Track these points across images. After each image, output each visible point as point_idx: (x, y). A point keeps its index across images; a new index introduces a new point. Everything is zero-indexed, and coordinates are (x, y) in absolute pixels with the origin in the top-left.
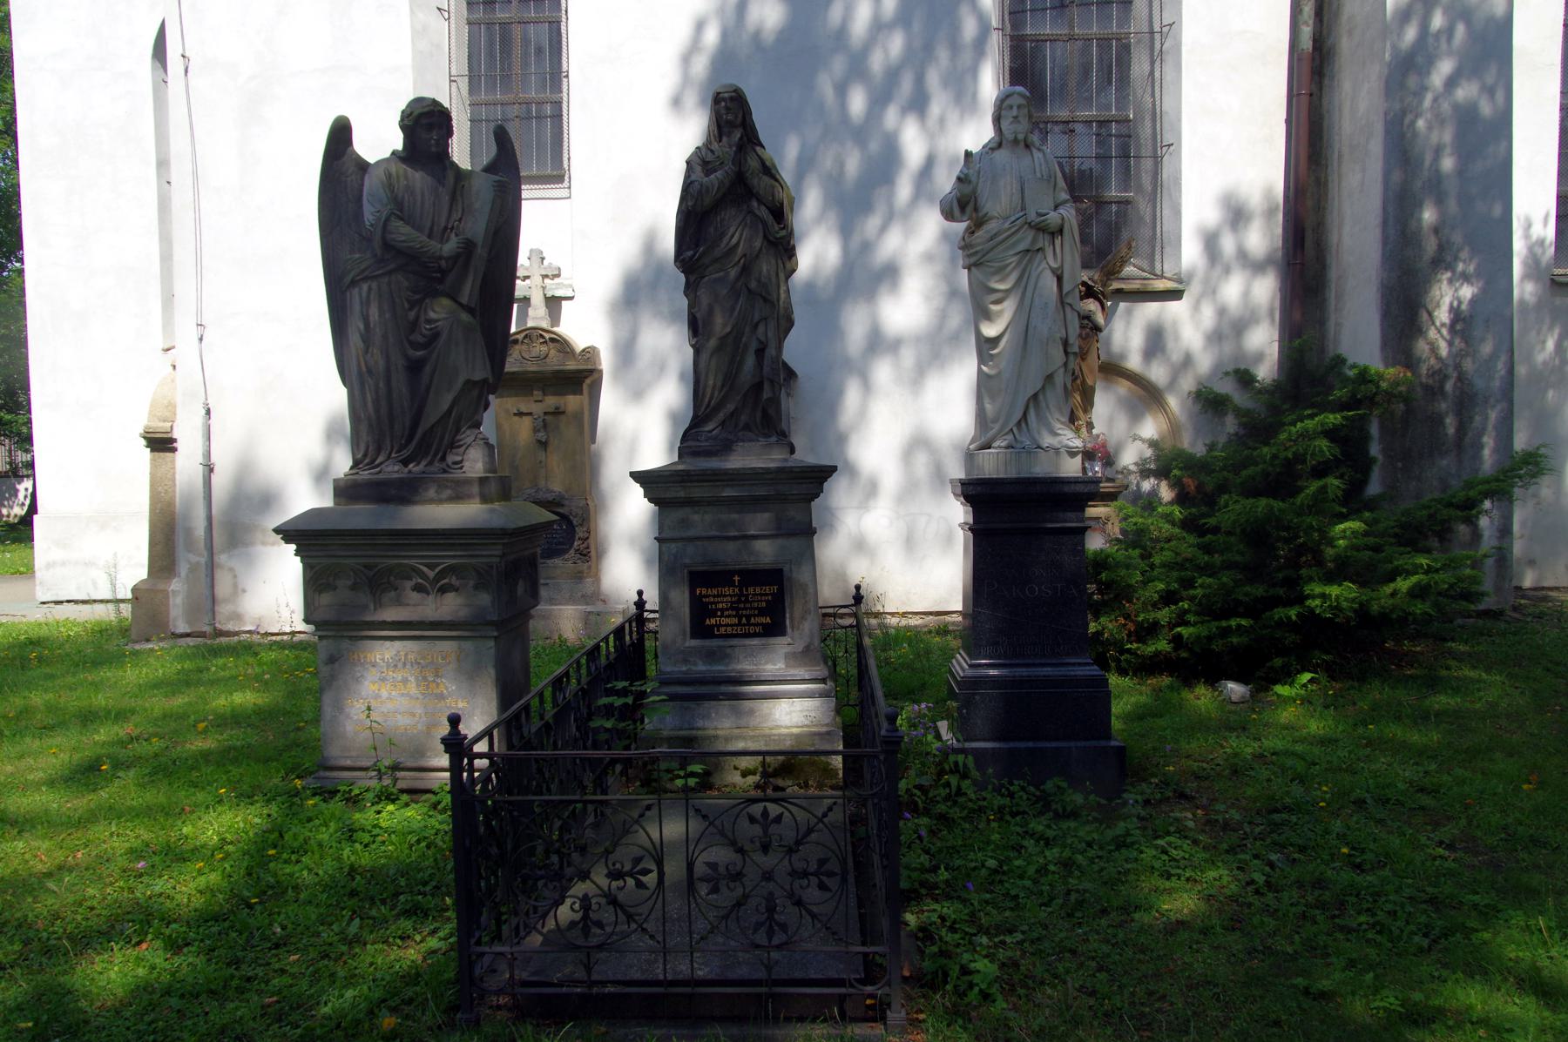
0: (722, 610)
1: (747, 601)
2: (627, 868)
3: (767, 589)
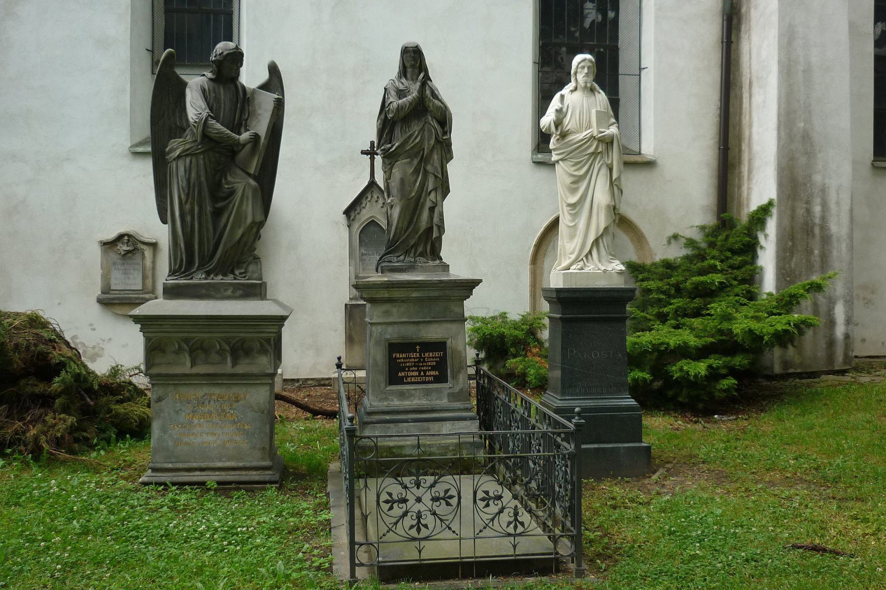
0: (409, 367)
1: (424, 361)
2: (442, 494)
3: (437, 354)
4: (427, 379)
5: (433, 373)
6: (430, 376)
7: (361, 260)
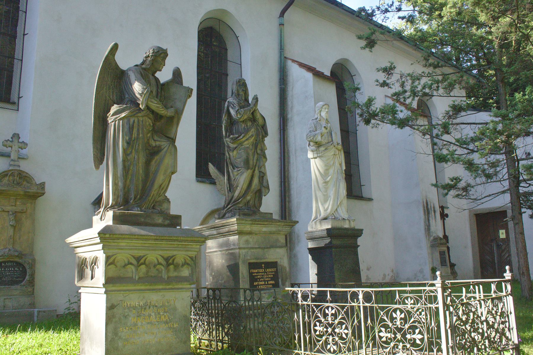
6: (271, 284)
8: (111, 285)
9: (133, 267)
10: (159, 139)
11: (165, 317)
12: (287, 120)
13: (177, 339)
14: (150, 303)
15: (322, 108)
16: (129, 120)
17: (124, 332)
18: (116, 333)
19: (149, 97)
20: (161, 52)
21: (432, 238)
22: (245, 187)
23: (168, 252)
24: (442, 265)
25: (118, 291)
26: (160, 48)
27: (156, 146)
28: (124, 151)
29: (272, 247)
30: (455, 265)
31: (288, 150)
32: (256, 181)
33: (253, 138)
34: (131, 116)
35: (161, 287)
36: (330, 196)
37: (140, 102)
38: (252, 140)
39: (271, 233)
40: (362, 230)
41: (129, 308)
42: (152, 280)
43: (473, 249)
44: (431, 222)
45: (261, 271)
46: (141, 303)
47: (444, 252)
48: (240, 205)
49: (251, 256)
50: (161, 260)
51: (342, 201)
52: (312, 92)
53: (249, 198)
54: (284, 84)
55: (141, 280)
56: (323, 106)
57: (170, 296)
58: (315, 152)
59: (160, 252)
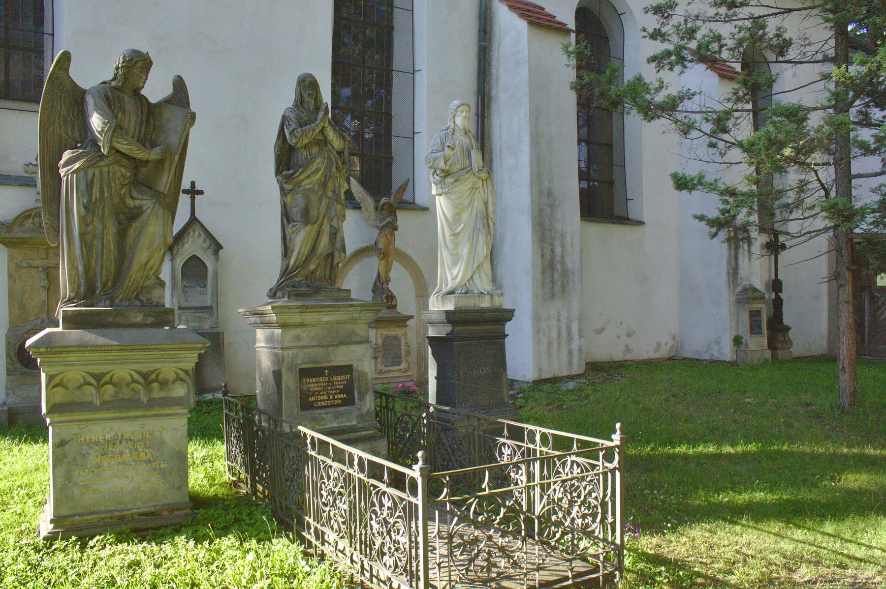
0: (319, 392)
4: (336, 402)
5: (341, 396)
6: (339, 399)
7: (184, 292)
8: (57, 415)
9: (92, 388)
10: (139, 196)
11: (146, 453)
12: (490, 100)
13: (167, 484)
14: (122, 435)
15: (456, 110)
16: (86, 174)
17: (81, 476)
18: (68, 478)
19: (112, 136)
20: (136, 59)
21: (739, 288)
22: (306, 251)
23: (146, 365)
24: (752, 334)
25: (69, 421)
26: (136, 53)
27: (135, 207)
28: (82, 219)
29: (342, 343)
30: (790, 328)
31: (491, 149)
32: (325, 240)
33: (320, 173)
34: (88, 167)
35: (138, 413)
36: (462, 256)
37: (101, 144)
38: (318, 176)
39: (339, 322)
40: (512, 311)
41: (88, 444)
42: (123, 404)
43: (829, 302)
44: (740, 261)
45: (322, 379)
46: (108, 437)
47: (760, 311)
48: (297, 279)
49: (303, 359)
50: (136, 376)
51: (482, 263)
52: (526, 52)
53: (312, 267)
54: (485, 40)
55: (105, 406)
56: (458, 107)
57: (153, 425)
58: (439, 186)
59: (134, 367)
